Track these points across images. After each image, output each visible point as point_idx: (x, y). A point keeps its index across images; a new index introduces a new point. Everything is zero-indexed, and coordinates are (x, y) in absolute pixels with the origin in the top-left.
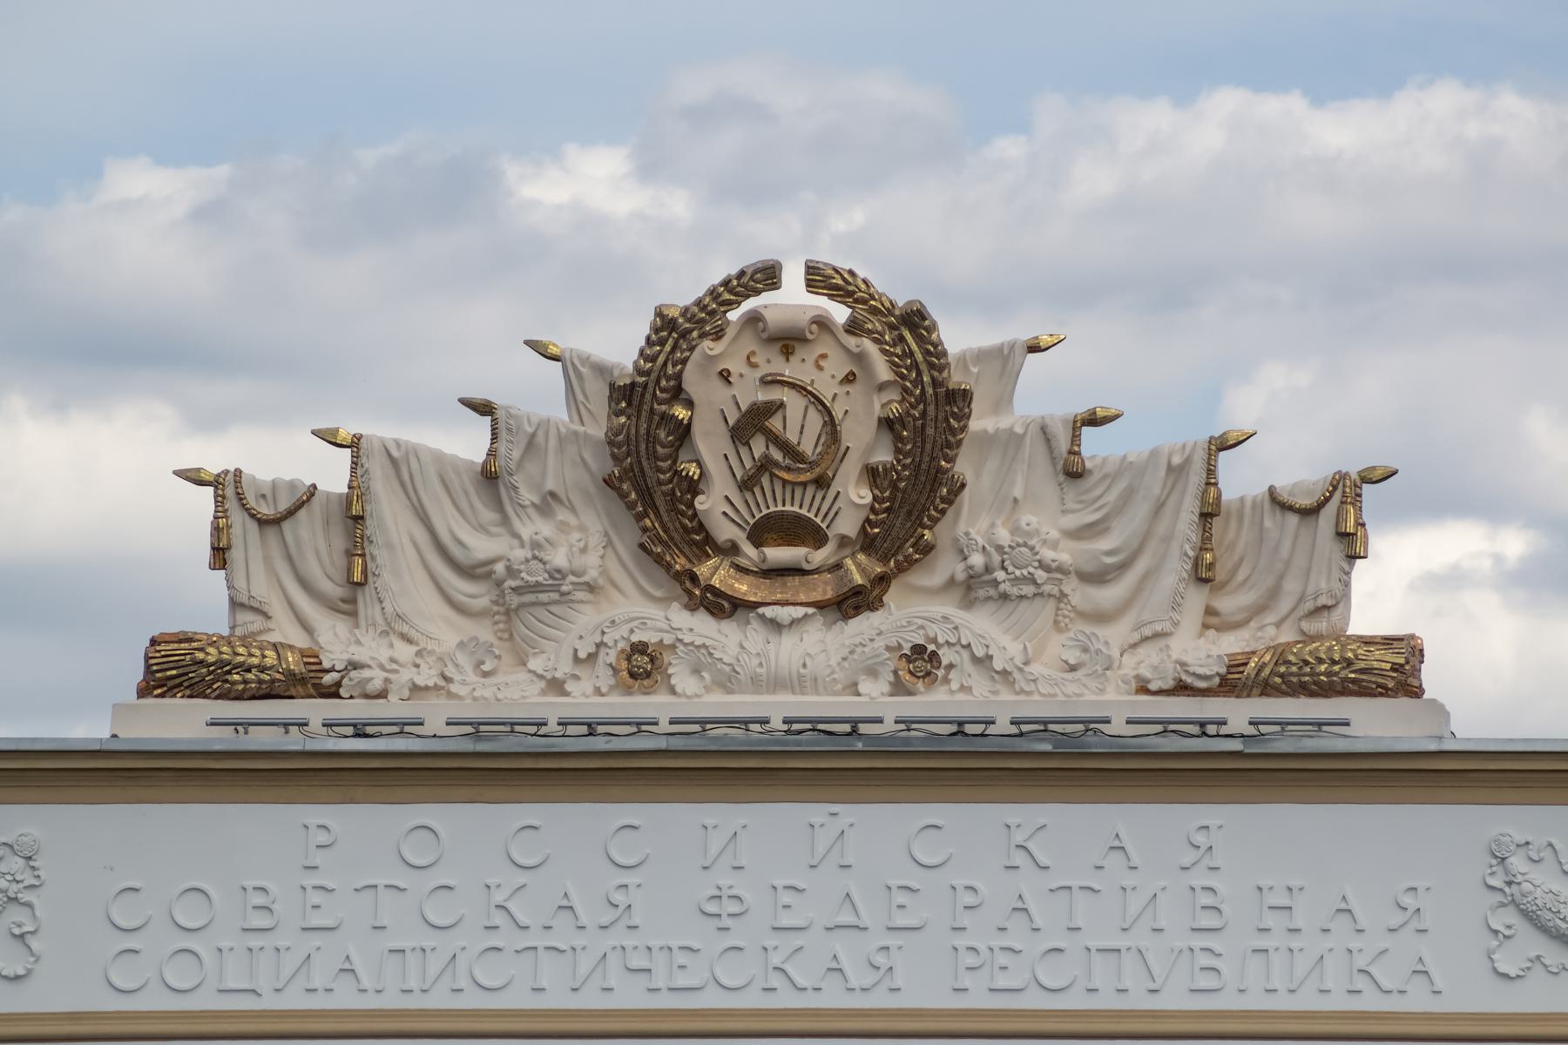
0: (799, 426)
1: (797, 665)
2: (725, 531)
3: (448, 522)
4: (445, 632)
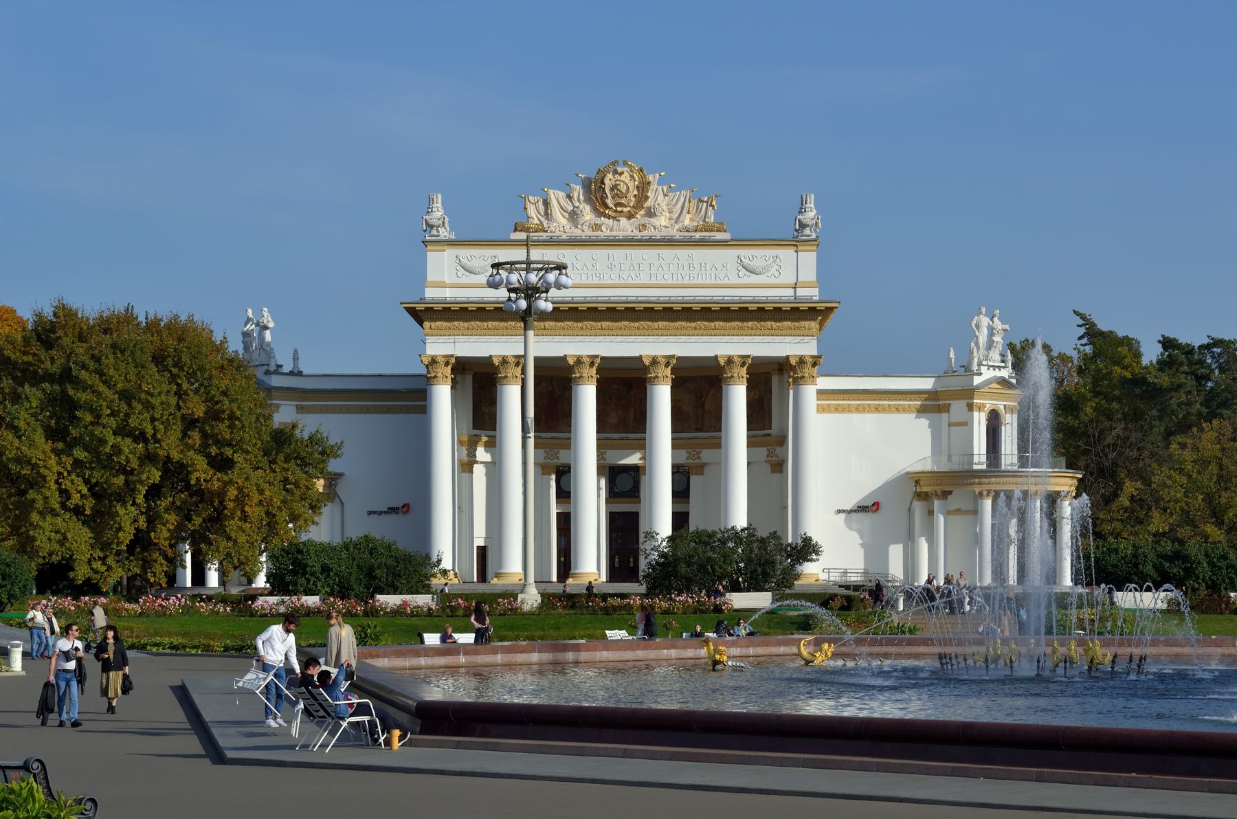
0: (623, 188)
1: (625, 227)
2: (611, 205)
3: (562, 202)
4: (564, 221)
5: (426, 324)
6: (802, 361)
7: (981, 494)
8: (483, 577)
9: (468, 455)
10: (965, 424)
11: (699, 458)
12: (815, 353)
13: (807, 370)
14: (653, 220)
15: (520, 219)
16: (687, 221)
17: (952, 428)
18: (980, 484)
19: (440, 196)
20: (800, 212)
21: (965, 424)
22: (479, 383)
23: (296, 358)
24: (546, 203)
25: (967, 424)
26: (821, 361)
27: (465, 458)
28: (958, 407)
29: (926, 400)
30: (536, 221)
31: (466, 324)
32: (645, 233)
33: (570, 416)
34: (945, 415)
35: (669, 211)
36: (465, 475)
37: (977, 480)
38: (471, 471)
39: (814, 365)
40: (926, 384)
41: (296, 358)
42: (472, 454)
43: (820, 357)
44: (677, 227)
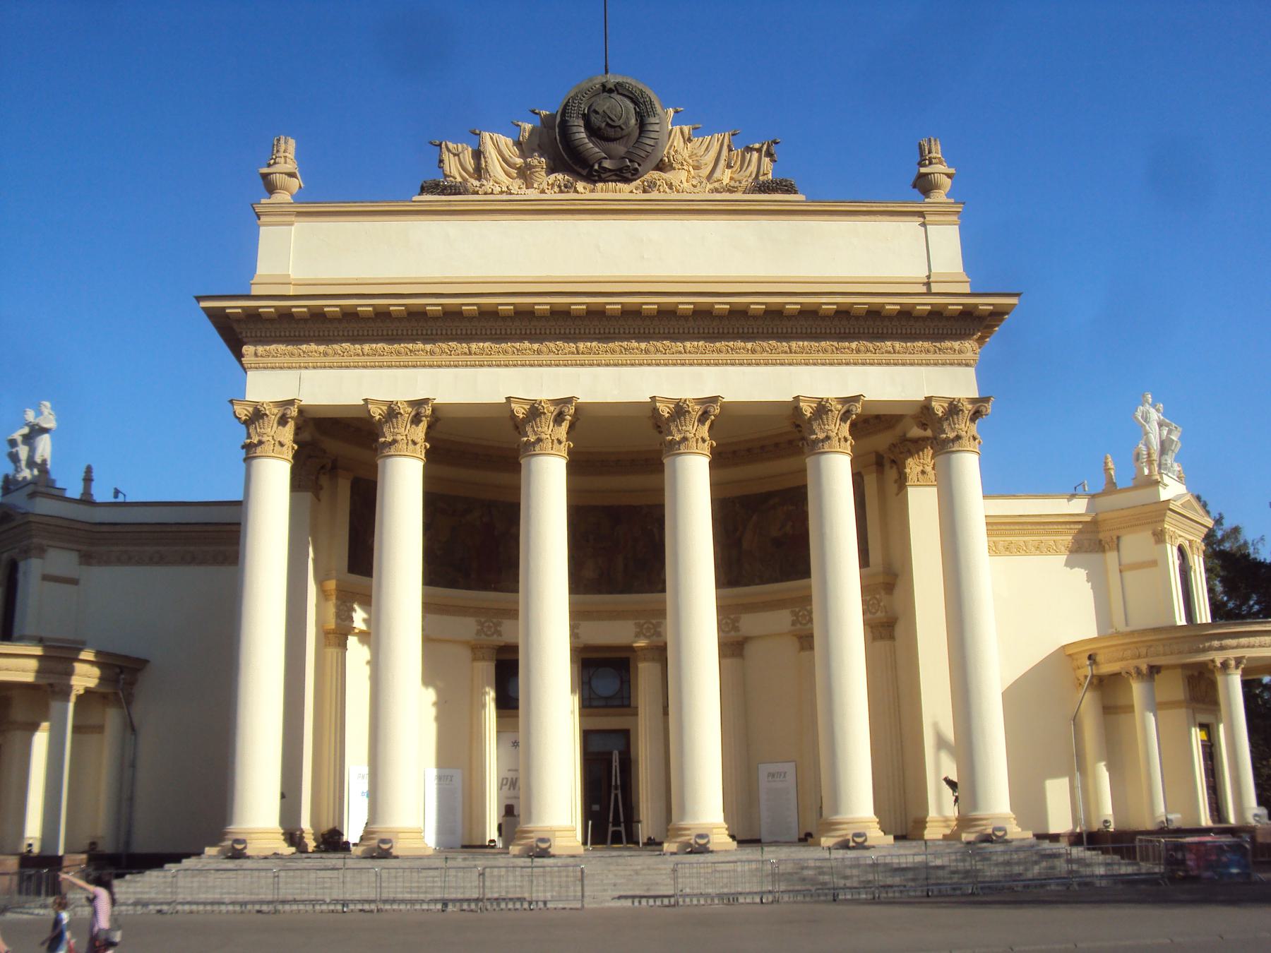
5: (248, 349)
6: (954, 408)
7: (1225, 665)
8: (1127, 624)
9: (338, 616)
10: (1154, 563)
11: (500, 634)
12: (975, 394)
13: (964, 426)
14: (668, 176)
15: (432, 176)
16: (726, 176)
17: (1128, 575)
18: (1222, 648)
19: (292, 143)
20: (921, 165)
21: (1154, 563)
22: (336, 457)
23: (88, 479)
24: (478, 154)
25: (1157, 563)
26: (989, 408)
27: (332, 624)
28: (1135, 544)
29: (1080, 532)
30: (459, 179)
31: (322, 348)
32: (654, 195)
33: (517, 575)
34: (1111, 557)
35: (691, 154)
36: (332, 652)
37: (1216, 643)
38: (343, 646)
39: (976, 415)
40: (1079, 506)
41: (88, 479)
42: (345, 617)
43: (984, 400)
44: (709, 186)
